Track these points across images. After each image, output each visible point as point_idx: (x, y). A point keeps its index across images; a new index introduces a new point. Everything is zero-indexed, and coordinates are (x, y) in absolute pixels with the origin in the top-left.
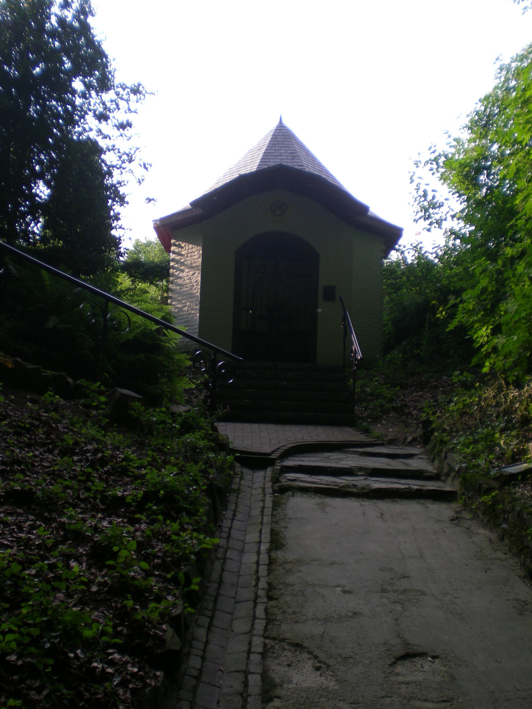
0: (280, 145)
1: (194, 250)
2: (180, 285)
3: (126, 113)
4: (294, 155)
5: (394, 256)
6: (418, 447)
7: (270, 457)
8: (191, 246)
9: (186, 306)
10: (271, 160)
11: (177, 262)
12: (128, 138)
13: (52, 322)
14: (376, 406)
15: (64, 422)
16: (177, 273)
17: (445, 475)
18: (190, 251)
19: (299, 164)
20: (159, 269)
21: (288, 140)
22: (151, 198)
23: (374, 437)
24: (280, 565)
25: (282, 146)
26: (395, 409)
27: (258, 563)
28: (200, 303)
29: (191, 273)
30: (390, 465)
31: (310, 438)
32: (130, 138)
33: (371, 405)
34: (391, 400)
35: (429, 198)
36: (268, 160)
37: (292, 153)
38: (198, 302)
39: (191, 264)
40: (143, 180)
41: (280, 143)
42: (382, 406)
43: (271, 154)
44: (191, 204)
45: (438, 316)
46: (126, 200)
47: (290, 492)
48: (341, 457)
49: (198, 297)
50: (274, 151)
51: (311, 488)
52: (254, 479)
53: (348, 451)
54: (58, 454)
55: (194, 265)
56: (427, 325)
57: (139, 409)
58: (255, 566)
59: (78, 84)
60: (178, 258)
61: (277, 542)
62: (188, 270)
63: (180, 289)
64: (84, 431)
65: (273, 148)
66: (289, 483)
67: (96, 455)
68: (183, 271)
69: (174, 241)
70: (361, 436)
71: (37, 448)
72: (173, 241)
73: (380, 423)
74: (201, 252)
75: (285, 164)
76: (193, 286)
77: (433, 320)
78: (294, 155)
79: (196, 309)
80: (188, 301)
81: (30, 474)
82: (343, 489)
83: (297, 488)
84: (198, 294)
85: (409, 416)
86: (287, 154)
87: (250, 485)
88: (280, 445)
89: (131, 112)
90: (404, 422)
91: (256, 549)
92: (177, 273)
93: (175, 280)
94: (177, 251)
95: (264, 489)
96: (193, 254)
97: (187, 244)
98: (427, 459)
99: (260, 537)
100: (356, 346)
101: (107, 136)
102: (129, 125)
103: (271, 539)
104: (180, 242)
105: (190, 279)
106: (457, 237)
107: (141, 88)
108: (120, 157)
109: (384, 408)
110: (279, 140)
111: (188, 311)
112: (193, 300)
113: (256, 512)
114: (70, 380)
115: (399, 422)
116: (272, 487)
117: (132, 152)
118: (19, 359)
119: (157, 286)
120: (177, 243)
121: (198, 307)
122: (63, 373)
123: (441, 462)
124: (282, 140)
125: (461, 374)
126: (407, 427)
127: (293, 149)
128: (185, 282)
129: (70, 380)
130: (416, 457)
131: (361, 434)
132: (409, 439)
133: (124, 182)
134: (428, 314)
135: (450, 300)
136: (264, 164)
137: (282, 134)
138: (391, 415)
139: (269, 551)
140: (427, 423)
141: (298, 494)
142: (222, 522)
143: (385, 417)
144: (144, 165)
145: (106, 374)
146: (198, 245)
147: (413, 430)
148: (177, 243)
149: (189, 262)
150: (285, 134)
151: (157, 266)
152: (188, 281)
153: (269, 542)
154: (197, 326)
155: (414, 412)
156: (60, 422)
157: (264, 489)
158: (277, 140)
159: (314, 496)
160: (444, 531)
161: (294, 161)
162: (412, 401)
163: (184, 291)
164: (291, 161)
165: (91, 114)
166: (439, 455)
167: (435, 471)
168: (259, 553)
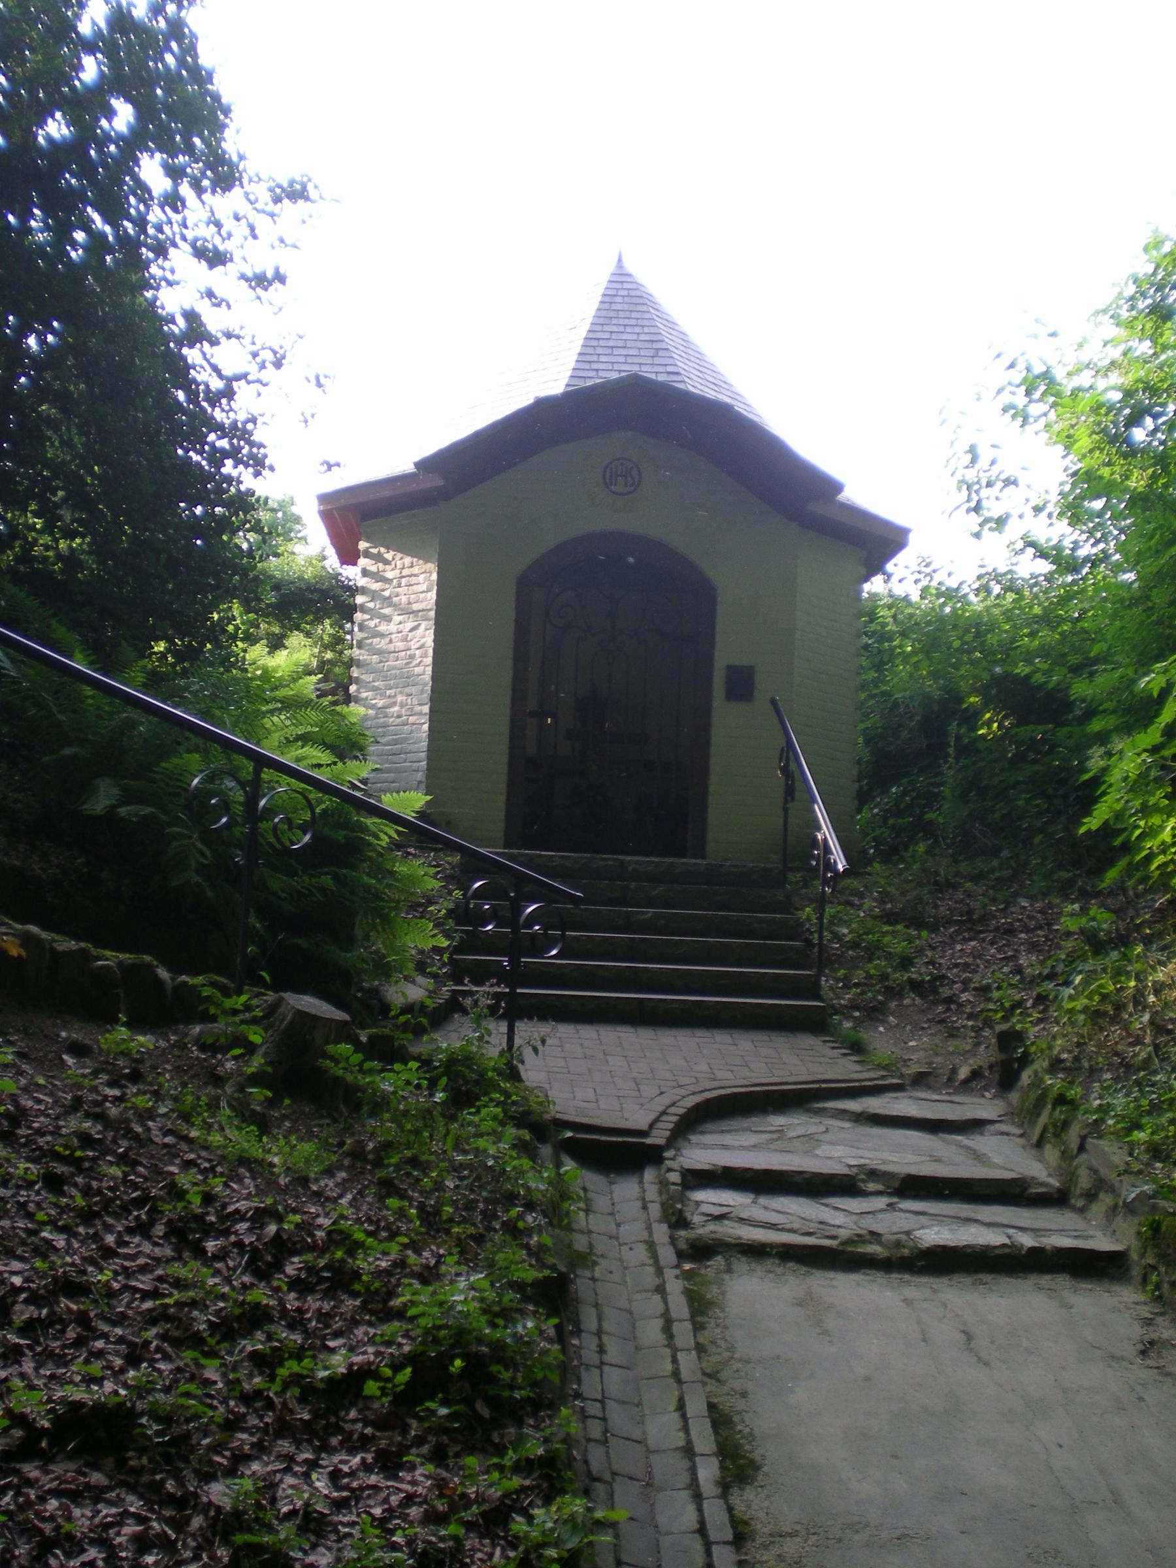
0: (622, 322)
1: (416, 570)
2: (379, 652)
3: (273, 247)
4: (656, 346)
5: (875, 585)
6: (987, 1094)
7: (648, 1141)
8: (408, 560)
9: (394, 704)
10: (603, 359)
11: (374, 596)
12: (277, 310)
13: (103, 797)
14: (869, 976)
15: (163, 1110)
16: (372, 624)
17: (1081, 1195)
18: (406, 572)
19: (670, 369)
20: (316, 596)
21: (640, 308)
22: (332, 462)
23: (879, 1067)
24: (765, 1547)
25: (626, 322)
26: (916, 986)
27: (702, 1530)
28: (433, 700)
29: (409, 625)
30: (938, 1160)
31: (729, 1075)
32: (280, 310)
33: (859, 976)
34: (906, 963)
35: (983, 462)
36: (595, 358)
37: (652, 341)
38: (426, 696)
39: (409, 603)
40: (313, 416)
41: (621, 314)
42: (885, 977)
43: (602, 343)
44: (417, 465)
45: (981, 732)
46: (267, 462)
47: (719, 1258)
48: (812, 1129)
49: (425, 684)
50: (607, 336)
51: (771, 1245)
52: (617, 1208)
53: (825, 1109)
54: (166, 1236)
55: (415, 607)
56: (951, 750)
57: (348, 1058)
58: (698, 1546)
59: (151, 170)
60: (376, 586)
61: (738, 1467)
62: (400, 618)
63: (381, 662)
64: (216, 1138)
65: (606, 328)
66: (711, 1227)
67: (262, 1227)
68: (388, 619)
69: (367, 545)
70: (845, 1061)
71: (110, 1220)
72: (363, 545)
73: (883, 1022)
74: (434, 576)
75: (653, 376)
76: (412, 657)
77: (966, 741)
78: (656, 347)
79: (421, 714)
80: (400, 693)
81: (106, 1328)
82: (851, 1249)
83: (736, 1245)
84: (427, 677)
85: (953, 1007)
86: (639, 345)
87: (612, 1229)
88: (666, 1100)
89: (286, 245)
90: (942, 1022)
91: (686, 1478)
92: (372, 624)
93: (367, 638)
94: (373, 569)
95: (651, 1246)
96: (413, 580)
97: (399, 555)
98: (1022, 1136)
99: (686, 1428)
100: (826, 832)
101: (223, 300)
102: (280, 278)
103: (718, 1443)
104: (382, 550)
105: (405, 639)
106: (1042, 554)
107: (310, 187)
108: (255, 355)
109: (891, 983)
110: (619, 307)
111: (399, 716)
112: (413, 690)
113: (651, 1332)
114: (163, 974)
115: (929, 1020)
116: (673, 1240)
117: (287, 346)
118: (34, 929)
119: (308, 635)
120: (374, 551)
121: (426, 709)
122: (147, 958)
123: (1065, 1155)
124: (626, 307)
125: (1084, 910)
126: (951, 1036)
127: (652, 330)
128: (391, 647)
129: (163, 974)
130: (991, 1128)
131: (845, 1055)
132: (963, 1073)
133: (262, 415)
134: (955, 724)
135: (1091, 758)
136: (587, 366)
137: (625, 293)
138: (907, 1002)
139: (725, 1488)
140: (1009, 1039)
141: (741, 1264)
142: (579, 1381)
143: (893, 1005)
144: (317, 378)
145: (264, 974)
146: (427, 561)
147: (968, 1048)
148: (374, 551)
149: (404, 599)
150: (632, 293)
151: (311, 588)
152: (400, 645)
153: (715, 1454)
154: (424, 755)
155: (965, 997)
156: (151, 1114)
157: (651, 1246)
158: (614, 307)
159: (779, 1270)
160: (1141, 1399)
161: (657, 361)
162: (956, 965)
163: (391, 669)
164: (649, 361)
165: (186, 247)
166: (1057, 1136)
167: (1055, 1183)
168: (698, 1497)
